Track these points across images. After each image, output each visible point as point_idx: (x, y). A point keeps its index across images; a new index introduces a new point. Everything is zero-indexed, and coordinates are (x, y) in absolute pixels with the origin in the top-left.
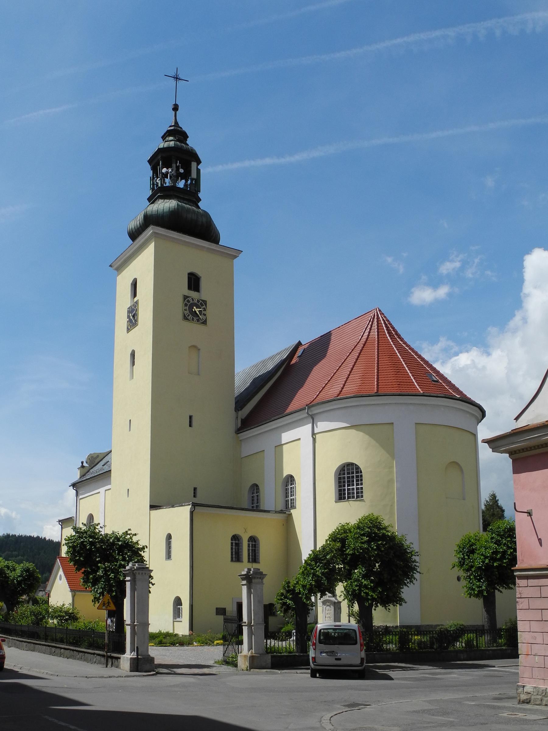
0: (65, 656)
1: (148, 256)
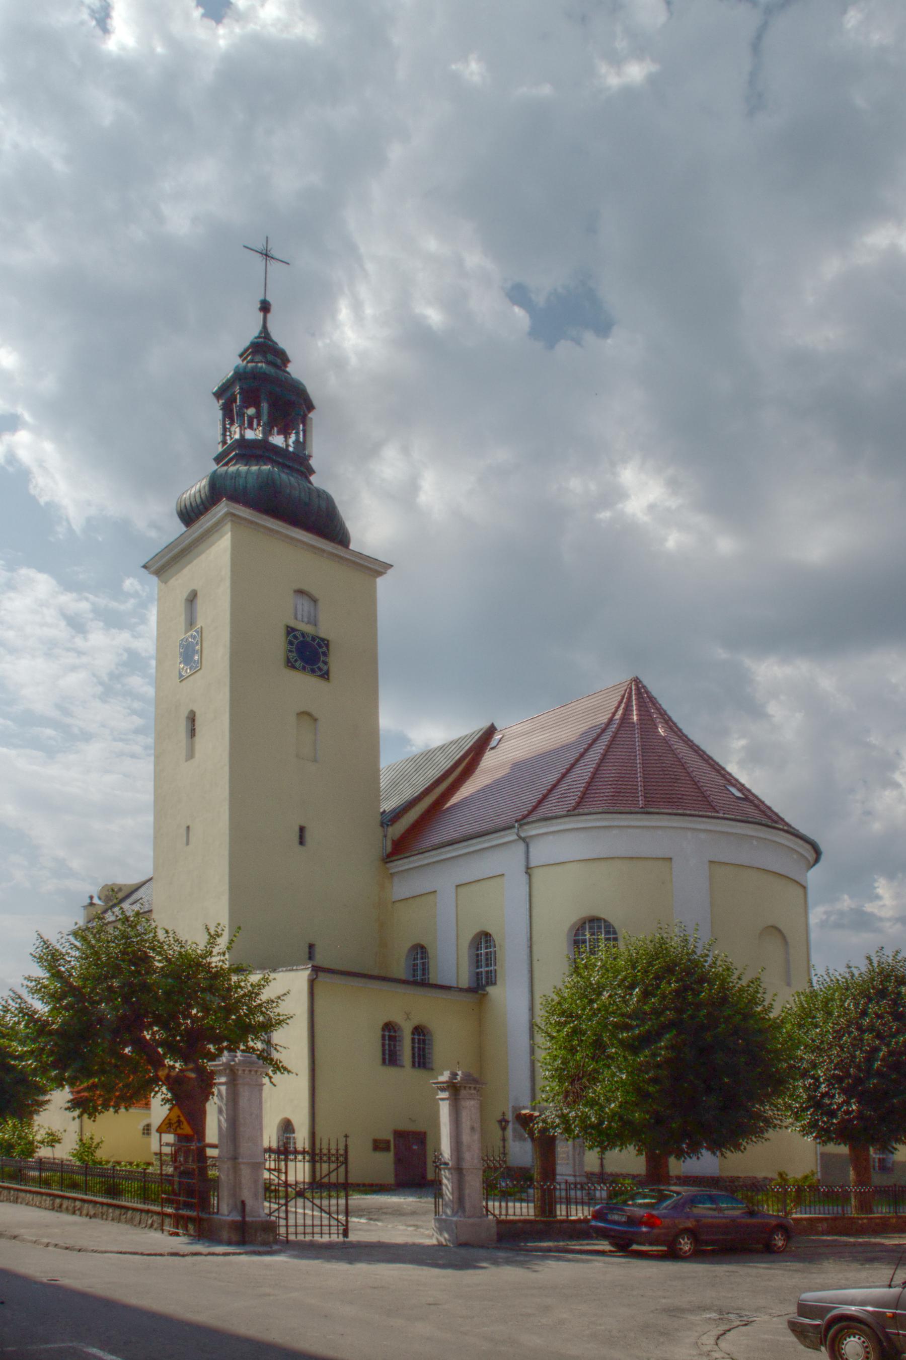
0: (84, 1212)
1: (220, 550)
